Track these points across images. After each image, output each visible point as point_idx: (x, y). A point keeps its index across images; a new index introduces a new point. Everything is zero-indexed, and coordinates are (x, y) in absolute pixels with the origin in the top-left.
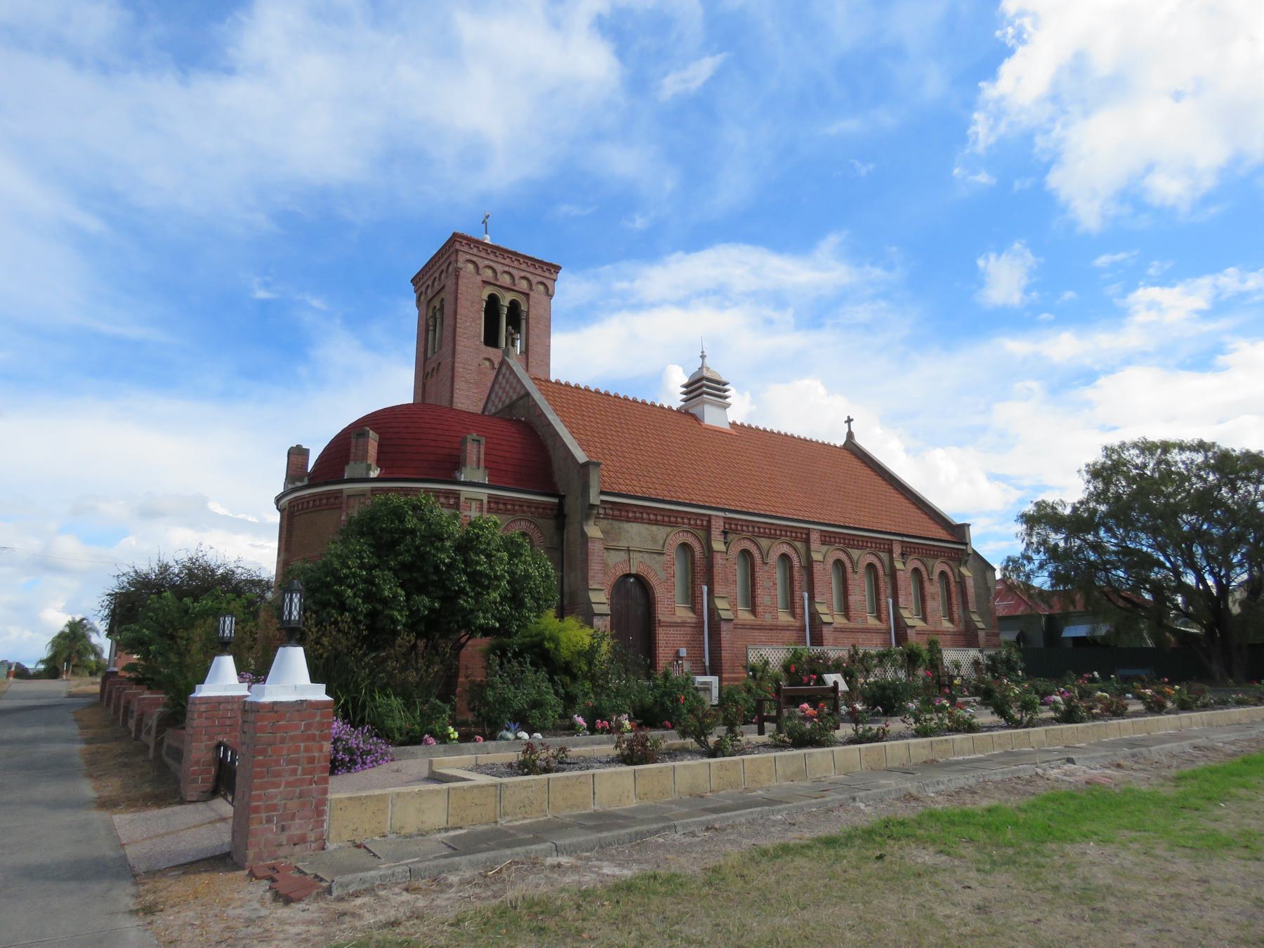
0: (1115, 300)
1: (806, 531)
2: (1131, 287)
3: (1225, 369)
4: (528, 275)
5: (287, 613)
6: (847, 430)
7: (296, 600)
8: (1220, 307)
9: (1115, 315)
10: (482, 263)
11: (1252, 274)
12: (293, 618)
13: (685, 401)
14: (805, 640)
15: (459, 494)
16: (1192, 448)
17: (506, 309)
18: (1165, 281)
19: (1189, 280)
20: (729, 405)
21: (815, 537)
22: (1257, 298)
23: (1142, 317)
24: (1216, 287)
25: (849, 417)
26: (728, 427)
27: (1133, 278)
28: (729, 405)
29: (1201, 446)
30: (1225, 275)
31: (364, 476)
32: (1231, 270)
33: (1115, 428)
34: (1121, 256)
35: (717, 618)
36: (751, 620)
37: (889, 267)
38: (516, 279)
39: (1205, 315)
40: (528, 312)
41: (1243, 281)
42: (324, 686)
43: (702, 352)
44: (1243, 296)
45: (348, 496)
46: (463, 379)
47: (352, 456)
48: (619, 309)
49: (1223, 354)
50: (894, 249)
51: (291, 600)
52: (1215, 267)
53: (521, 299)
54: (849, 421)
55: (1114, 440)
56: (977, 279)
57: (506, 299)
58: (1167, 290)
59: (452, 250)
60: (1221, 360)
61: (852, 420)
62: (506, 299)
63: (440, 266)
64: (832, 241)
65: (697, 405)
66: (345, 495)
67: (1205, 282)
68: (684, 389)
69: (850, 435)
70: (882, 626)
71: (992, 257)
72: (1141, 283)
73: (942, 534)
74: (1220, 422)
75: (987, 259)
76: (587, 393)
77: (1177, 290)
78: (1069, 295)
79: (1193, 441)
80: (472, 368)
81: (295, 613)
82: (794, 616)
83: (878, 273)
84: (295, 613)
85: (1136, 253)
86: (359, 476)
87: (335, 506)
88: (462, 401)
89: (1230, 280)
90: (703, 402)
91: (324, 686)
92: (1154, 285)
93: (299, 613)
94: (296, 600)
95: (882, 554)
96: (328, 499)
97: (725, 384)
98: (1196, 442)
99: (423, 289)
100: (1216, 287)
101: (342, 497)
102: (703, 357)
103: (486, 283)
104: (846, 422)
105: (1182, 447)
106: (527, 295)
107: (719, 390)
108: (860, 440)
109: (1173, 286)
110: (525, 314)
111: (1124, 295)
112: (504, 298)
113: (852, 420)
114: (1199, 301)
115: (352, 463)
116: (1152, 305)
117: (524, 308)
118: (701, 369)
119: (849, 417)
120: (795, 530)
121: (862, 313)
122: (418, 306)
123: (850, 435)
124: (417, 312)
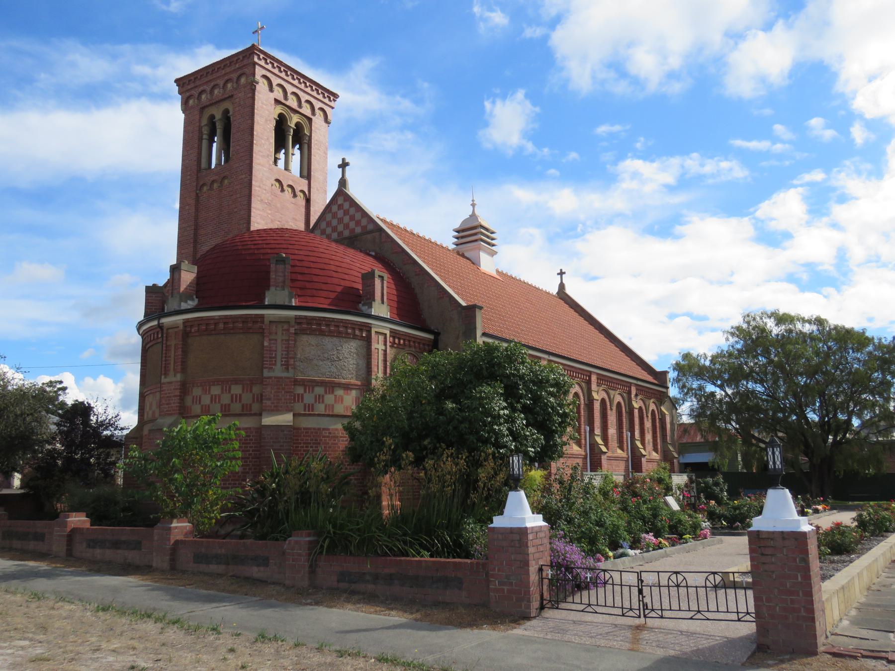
0: (608, 166)
1: (588, 374)
2: (621, 157)
3: (678, 237)
4: (312, 100)
5: (771, 463)
6: (560, 282)
7: (777, 453)
8: (684, 183)
9: (608, 179)
10: (275, 81)
11: (710, 161)
12: (777, 467)
13: (457, 245)
14: (587, 466)
15: (371, 328)
16: (809, 322)
17: (292, 131)
18: (647, 156)
19: (665, 158)
20: (496, 253)
21: (594, 378)
22: (711, 181)
23: (627, 184)
24: (682, 167)
25: (561, 270)
26: (494, 274)
27: (623, 150)
28: (496, 253)
29: (820, 322)
30: (691, 159)
31: (286, 303)
32: (695, 155)
33: (595, 278)
34: (617, 128)
35: (596, 451)
36: (577, 451)
37: (418, 102)
38: (289, 94)
39: (670, 189)
40: (310, 137)
41: (702, 165)
42: (85, 513)
43: (473, 201)
44: (700, 178)
45: (270, 322)
46: (259, 199)
47: (272, 282)
48: (139, 95)
49: (681, 224)
50: (426, 85)
51: (773, 453)
52: (684, 151)
53: (304, 123)
54: (561, 273)
55: (756, 308)
56: (481, 120)
57: (294, 119)
58: (648, 164)
59: (245, 62)
60: (678, 229)
61: (564, 273)
62: (294, 119)
63: (230, 72)
64: (367, 64)
65: (471, 250)
66: (266, 321)
67: (675, 161)
68: (456, 234)
69: (562, 286)
70: (624, 455)
71: (499, 103)
72: (630, 155)
73: (650, 378)
74: (673, 281)
75: (494, 103)
76: (411, 236)
77: (655, 165)
78: (573, 155)
79: (812, 316)
80: (267, 188)
81: (778, 463)
82: (580, 447)
83: (406, 104)
84: (778, 463)
85: (628, 127)
86: (281, 303)
87: (251, 331)
88: (258, 221)
89: (693, 163)
90: (479, 249)
91: (85, 513)
92: (639, 158)
93: (781, 463)
94: (777, 453)
95: (625, 394)
96: (225, 323)
97: (493, 233)
98: (814, 317)
99: (195, 93)
100: (682, 167)
101: (263, 322)
102: (473, 205)
103: (277, 102)
104: (558, 274)
105: (804, 321)
106: (310, 120)
107: (488, 237)
108: (569, 291)
109: (653, 161)
110: (307, 138)
111: (616, 162)
112: (291, 119)
113: (564, 273)
114: (669, 178)
115: (272, 289)
116: (635, 175)
117: (306, 132)
118: (473, 216)
119: (561, 270)
120: (573, 369)
121: (390, 142)
122: (184, 110)
123: (562, 286)
124: (183, 116)
